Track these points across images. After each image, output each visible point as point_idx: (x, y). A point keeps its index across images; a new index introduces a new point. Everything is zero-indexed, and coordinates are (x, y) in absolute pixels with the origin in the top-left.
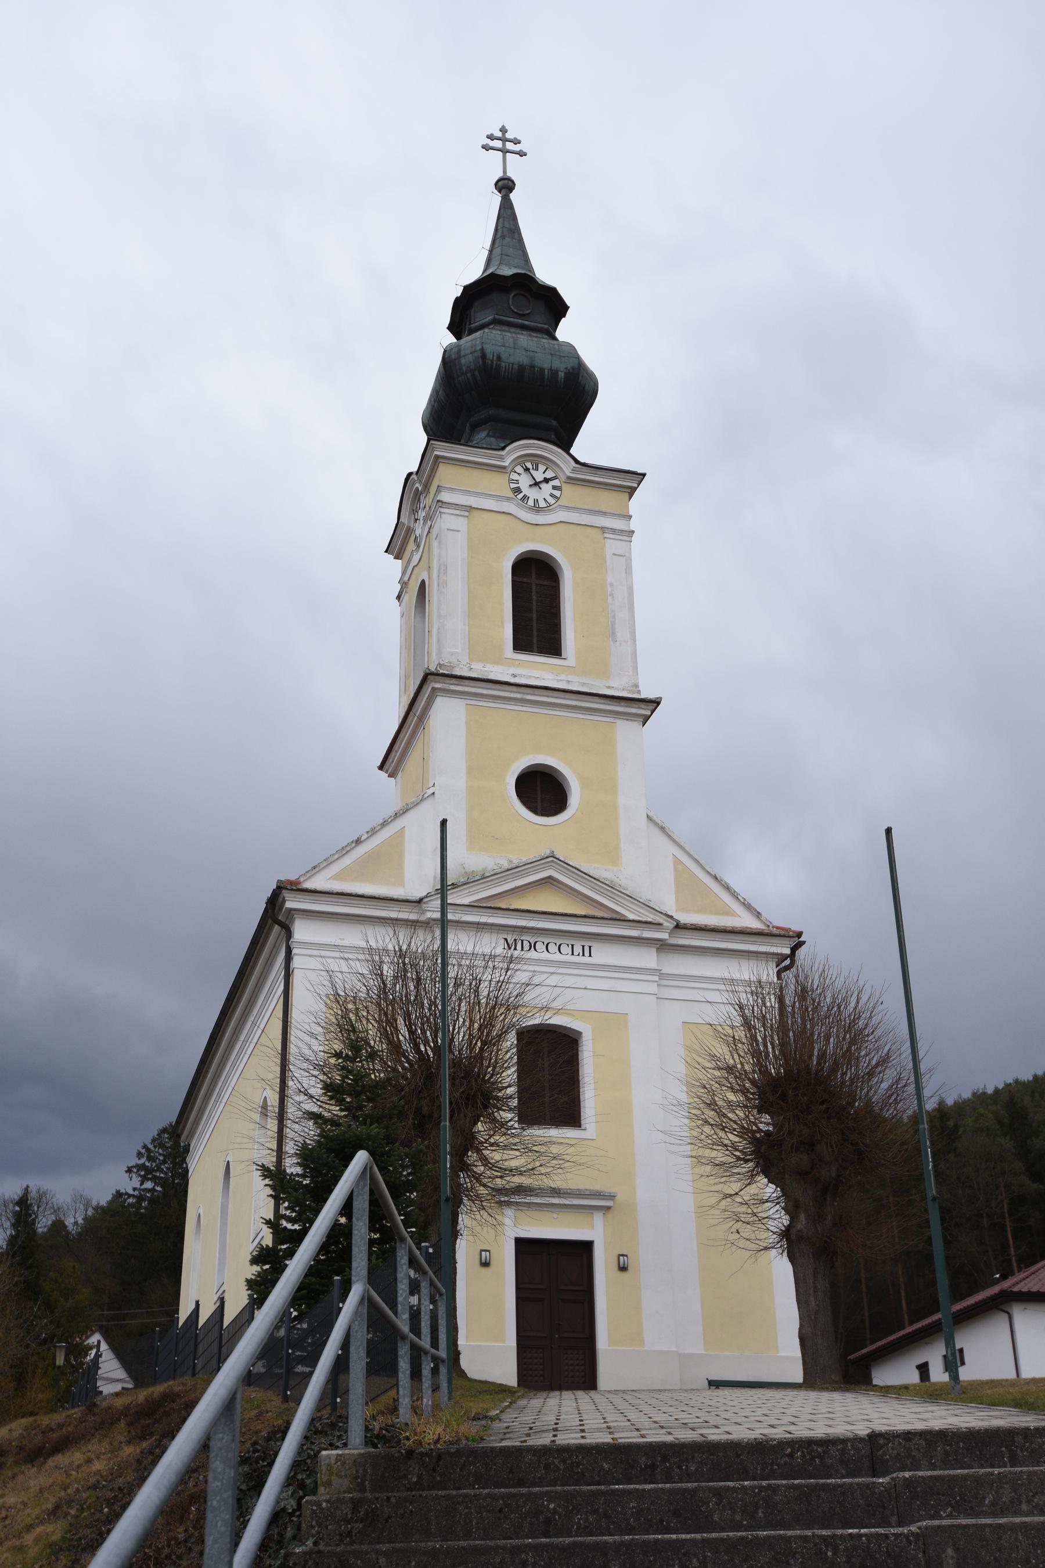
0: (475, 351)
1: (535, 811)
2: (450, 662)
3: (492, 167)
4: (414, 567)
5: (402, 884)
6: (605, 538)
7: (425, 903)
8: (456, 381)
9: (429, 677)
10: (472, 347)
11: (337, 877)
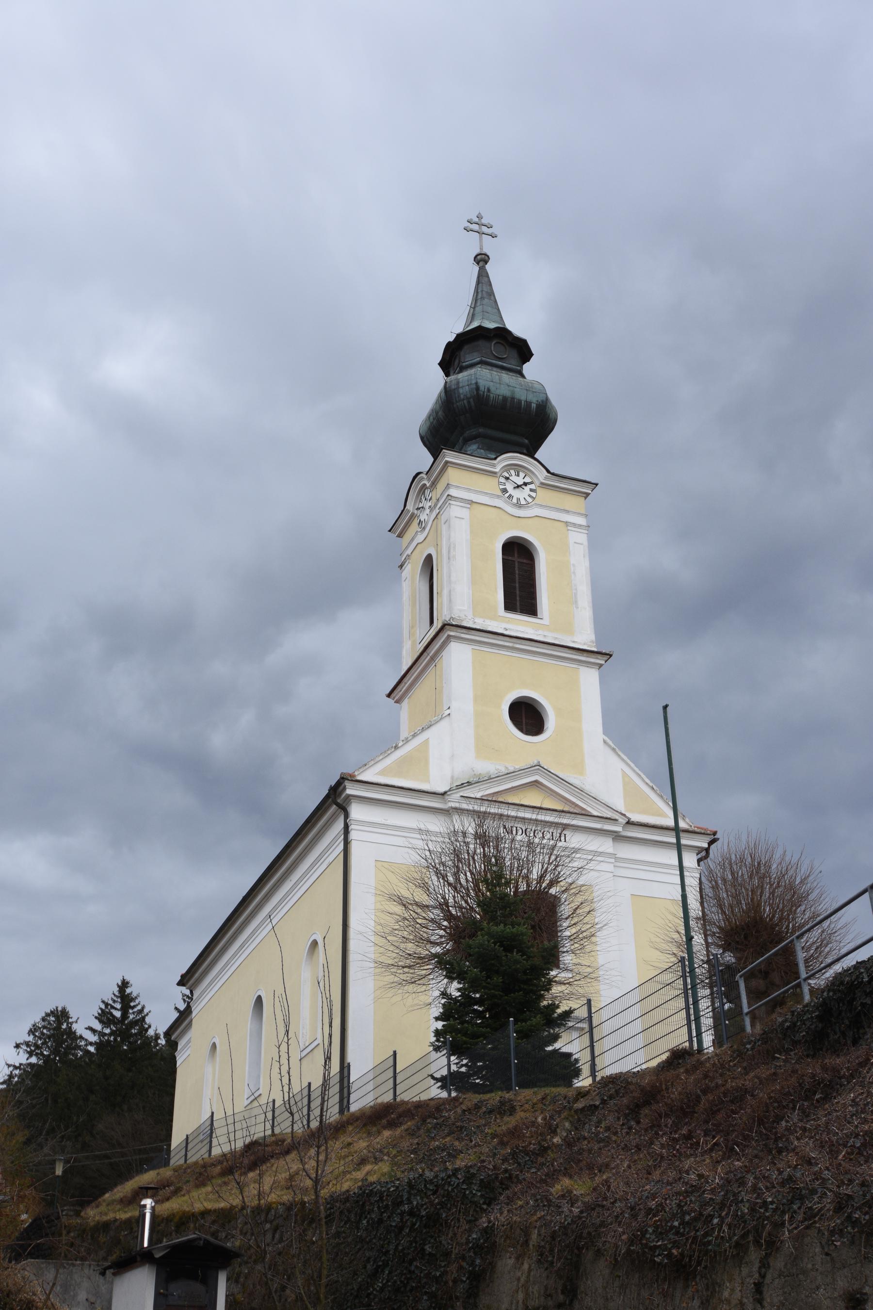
0: (471, 384)
1: (521, 730)
2: (459, 617)
3: (472, 245)
4: (418, 544)
6: (568, 530)
7: (448, 795)
8: (455, 406)
9: (446, 626)
10: (468, 381)
11: (382, 773)
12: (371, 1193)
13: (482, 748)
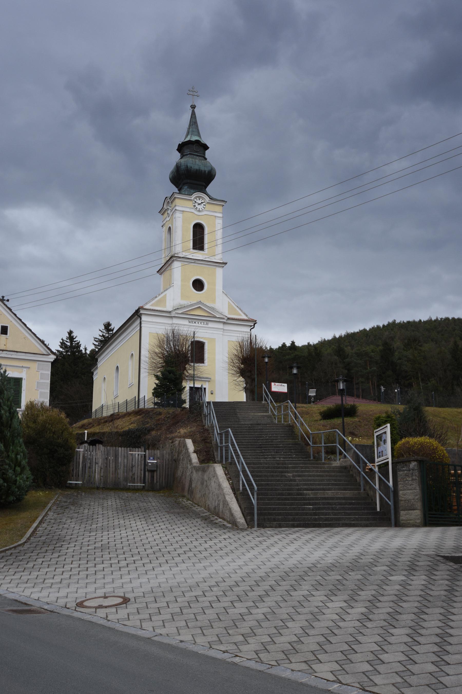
5: (165, 307)
11: (152, 305)
12: (130, 431)
13: (183, 296)
